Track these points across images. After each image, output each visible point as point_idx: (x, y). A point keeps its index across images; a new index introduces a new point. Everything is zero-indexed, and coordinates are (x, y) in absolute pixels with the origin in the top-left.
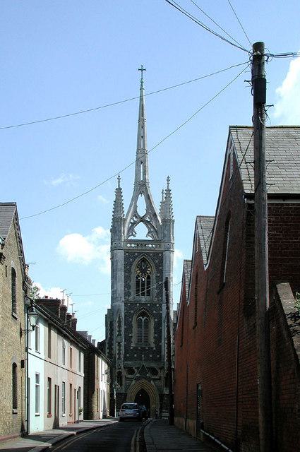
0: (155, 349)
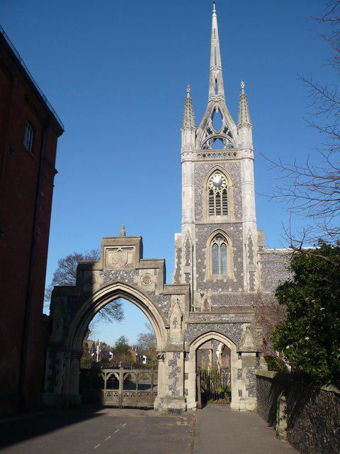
0: (235, 281)
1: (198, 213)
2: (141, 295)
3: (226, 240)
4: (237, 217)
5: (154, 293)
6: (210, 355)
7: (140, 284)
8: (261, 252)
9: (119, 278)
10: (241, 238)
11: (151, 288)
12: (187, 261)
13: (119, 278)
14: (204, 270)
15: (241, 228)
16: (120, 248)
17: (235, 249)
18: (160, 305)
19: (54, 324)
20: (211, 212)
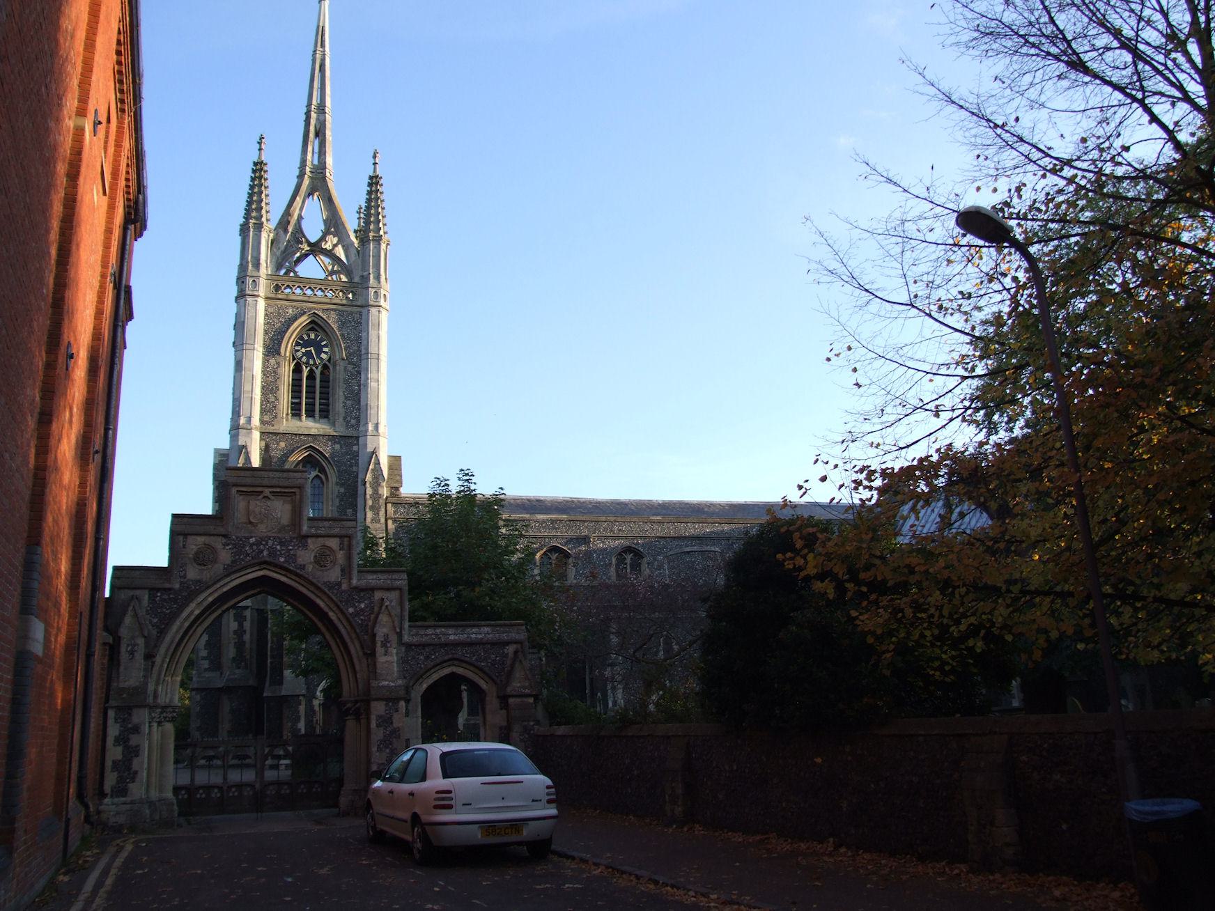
1: (268, 409)
2: (312, 588)
3: (323, 470)
4: (348, 426)
5: (339, 584)
6: (302, 708)
7: (310, 568)
8: (394, 500)
9: (265, 553)
10: (355, 469)
11: (334, 575)
13: (265, 553)
15: (355, 448)
16: (267, 491)
17: (342, 490)
18: (351, 610)
19: (123, 649)
20: (296, 411)
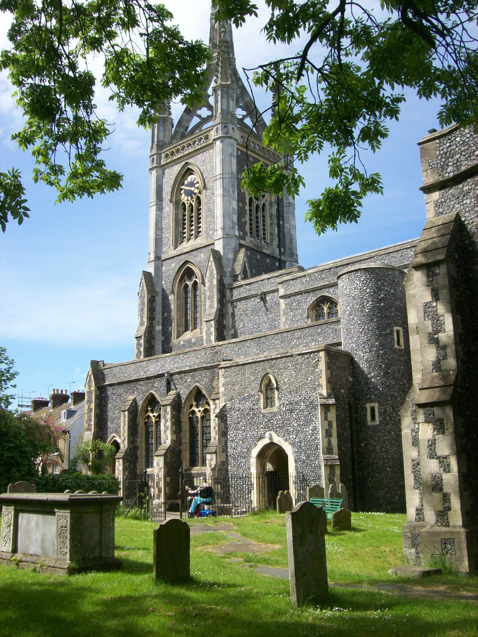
12: (142, 320)
14: (170, 329)
